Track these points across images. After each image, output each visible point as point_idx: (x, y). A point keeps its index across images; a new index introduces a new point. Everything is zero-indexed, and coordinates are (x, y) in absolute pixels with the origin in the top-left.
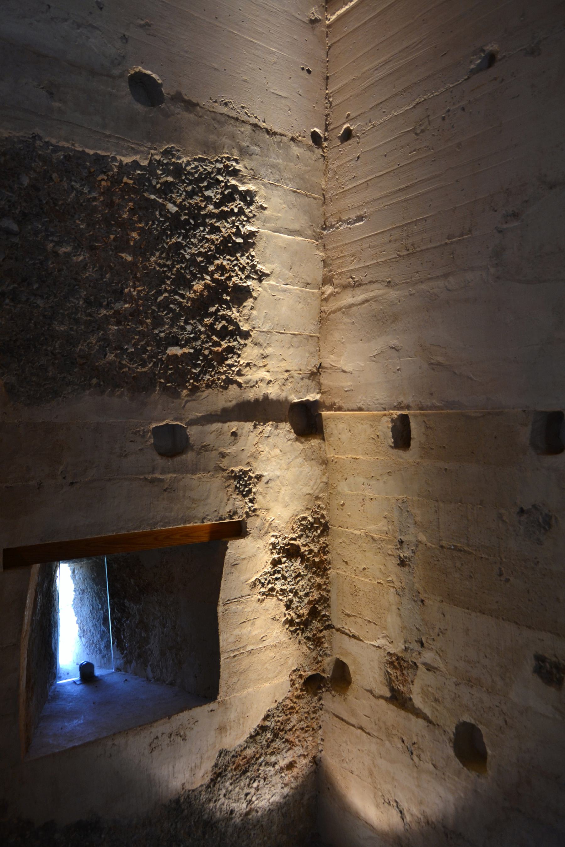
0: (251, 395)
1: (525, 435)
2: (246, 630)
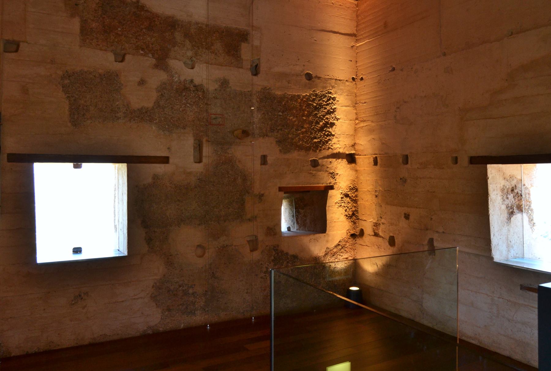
0: (335, 152)
1: (401, 160)
2: (334, 215)
